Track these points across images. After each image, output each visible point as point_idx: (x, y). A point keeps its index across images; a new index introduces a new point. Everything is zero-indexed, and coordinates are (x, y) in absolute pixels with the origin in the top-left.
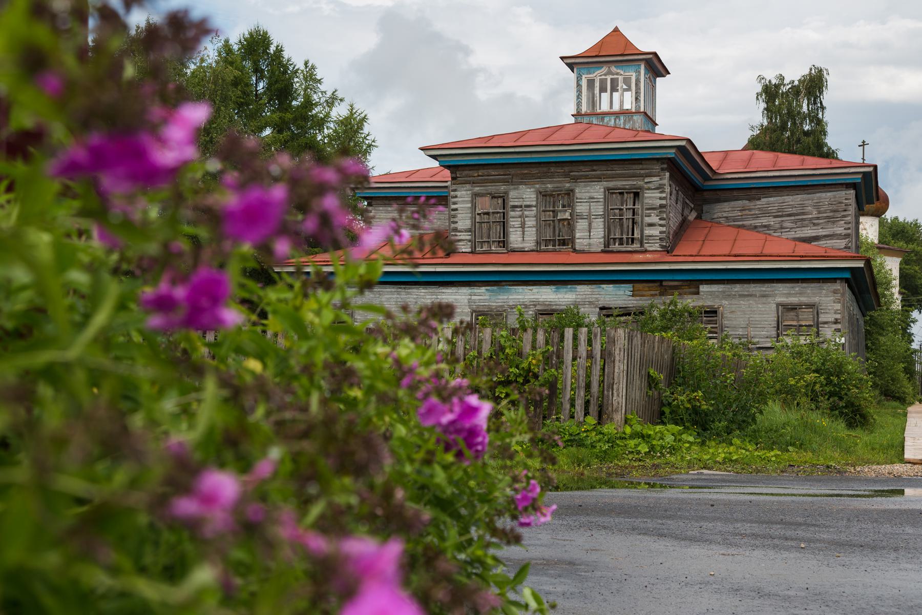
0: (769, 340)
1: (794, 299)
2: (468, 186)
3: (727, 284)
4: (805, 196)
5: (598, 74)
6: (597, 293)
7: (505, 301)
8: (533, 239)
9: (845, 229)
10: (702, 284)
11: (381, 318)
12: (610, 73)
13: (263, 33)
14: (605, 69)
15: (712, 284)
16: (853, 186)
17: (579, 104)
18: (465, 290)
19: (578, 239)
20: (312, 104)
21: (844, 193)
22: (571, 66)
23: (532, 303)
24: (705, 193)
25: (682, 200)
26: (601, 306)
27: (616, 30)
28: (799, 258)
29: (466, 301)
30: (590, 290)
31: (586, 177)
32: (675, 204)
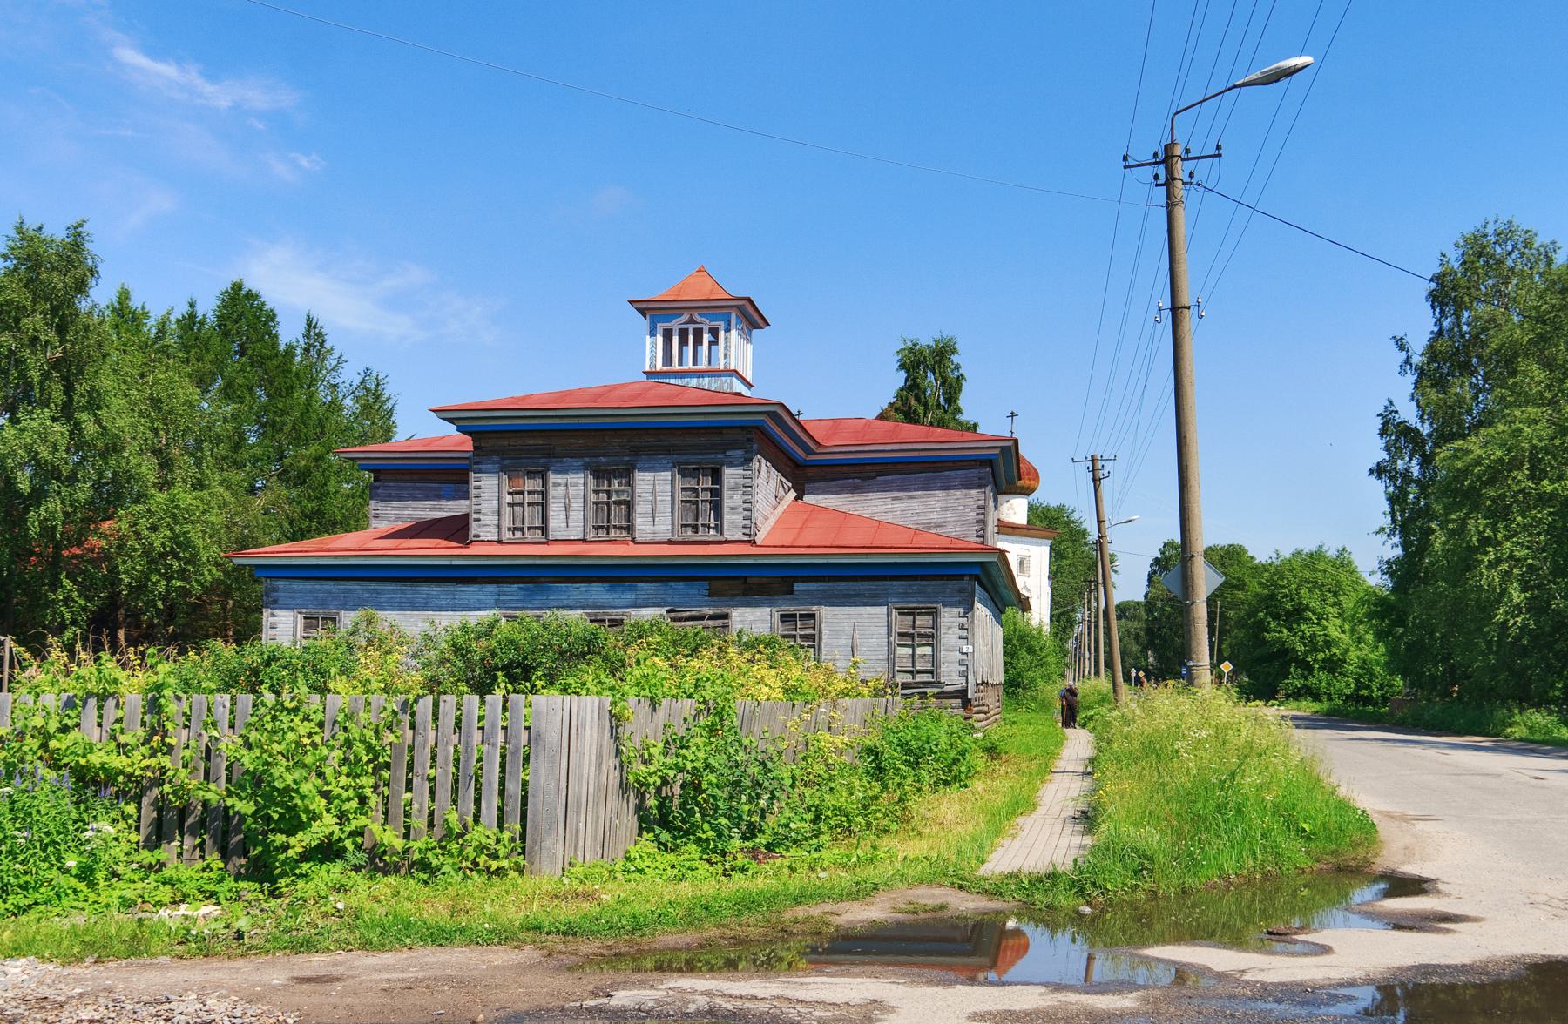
2: (495, 458)
8: (946, 620)
9: (977, 515)
11: (1093, 536)
12: (692, 321)
18: (491, 588)
20: (192, 316)
22: (643, 312)
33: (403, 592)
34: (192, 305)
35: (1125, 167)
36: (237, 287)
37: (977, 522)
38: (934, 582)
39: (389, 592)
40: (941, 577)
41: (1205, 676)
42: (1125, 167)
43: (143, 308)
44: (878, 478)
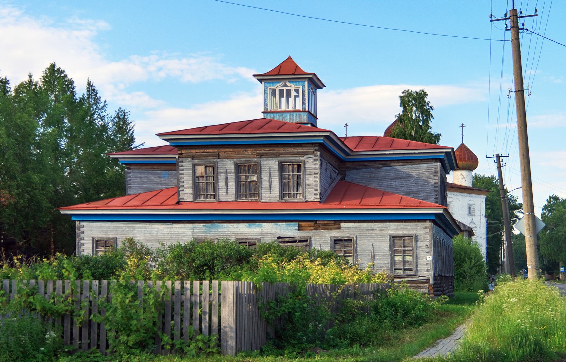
0: (395, 226)
1: (400, 232)
2: (190, 159)
3: (358, 222)
4: (410, 166)
5: (278, 87)
6: (275, 228)
7: (216, 233)
9: (435, 187)
10: (342, 223)
12: (286, 86)
14: (281, 84)
16: (441, 160)
17: (266, 105)
18: (189, 226)
19: (220, 284)
20: (31, 81)
21: (434, 164)
22: (261, 81)
23: (233, 234)
24: (347, 164)
25: (330, 168)
26: (278, 236)
27: (290, 58)
28: (402, 207)
29: (190, 233)
30: (270, 226)
31: (267, 154)
32: (325, 172)
33: (145, 228)
34: (30, 76)
35: (491, 21)
36: (53, 66)
37: (435, 191)
38: (411, 223)
39: (139, 228)
40: (414, 221)
41: (532, 274)
42: (491, 21)
43: (6, 79)
44: (383, 168)
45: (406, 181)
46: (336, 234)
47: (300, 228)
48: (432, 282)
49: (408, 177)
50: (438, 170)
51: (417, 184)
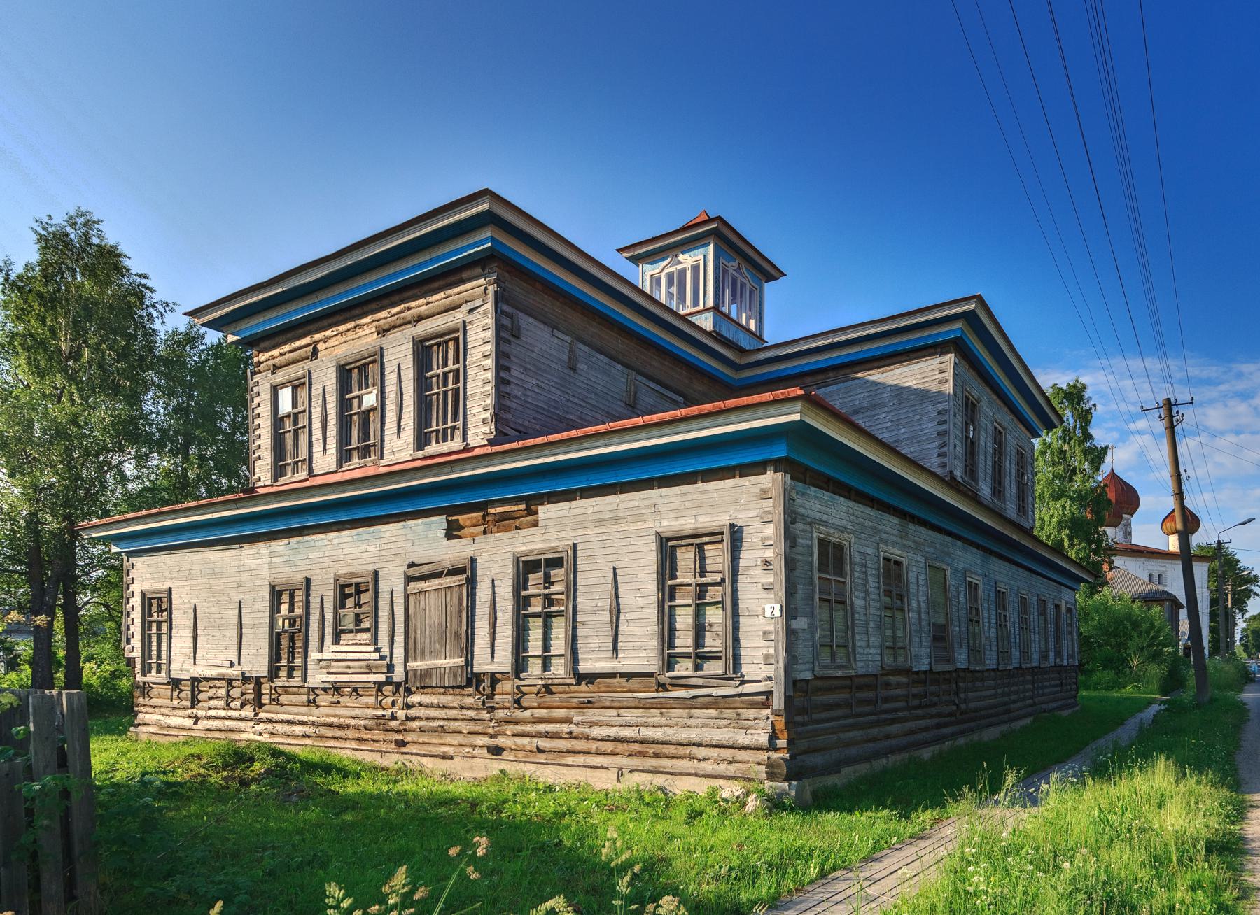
9: (939, 423)
13: (242, 442)
15: (693, 421)
45: (869, 417)
46: (529, 542)
47: (452, 532)
48: (778, 702)
49: (875, 406)
50: (947, 374)
51: (895, 423)
